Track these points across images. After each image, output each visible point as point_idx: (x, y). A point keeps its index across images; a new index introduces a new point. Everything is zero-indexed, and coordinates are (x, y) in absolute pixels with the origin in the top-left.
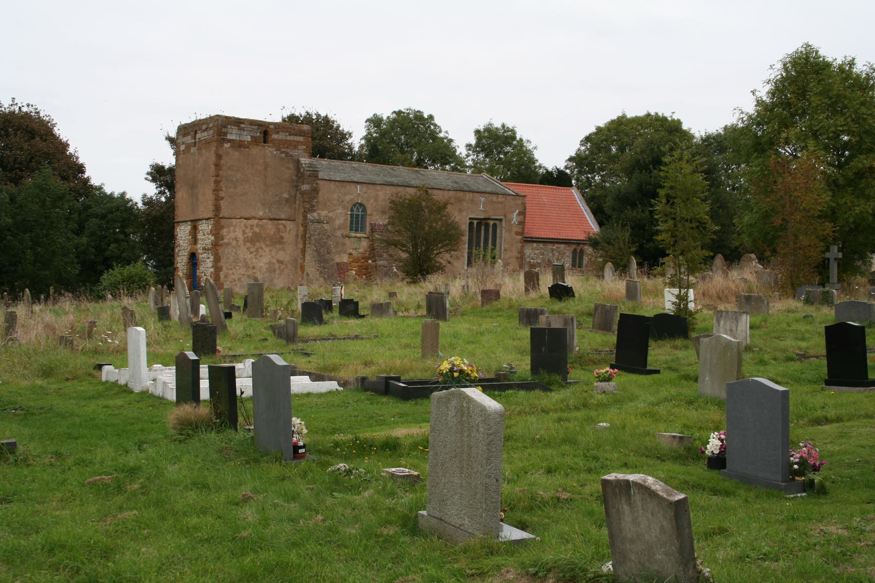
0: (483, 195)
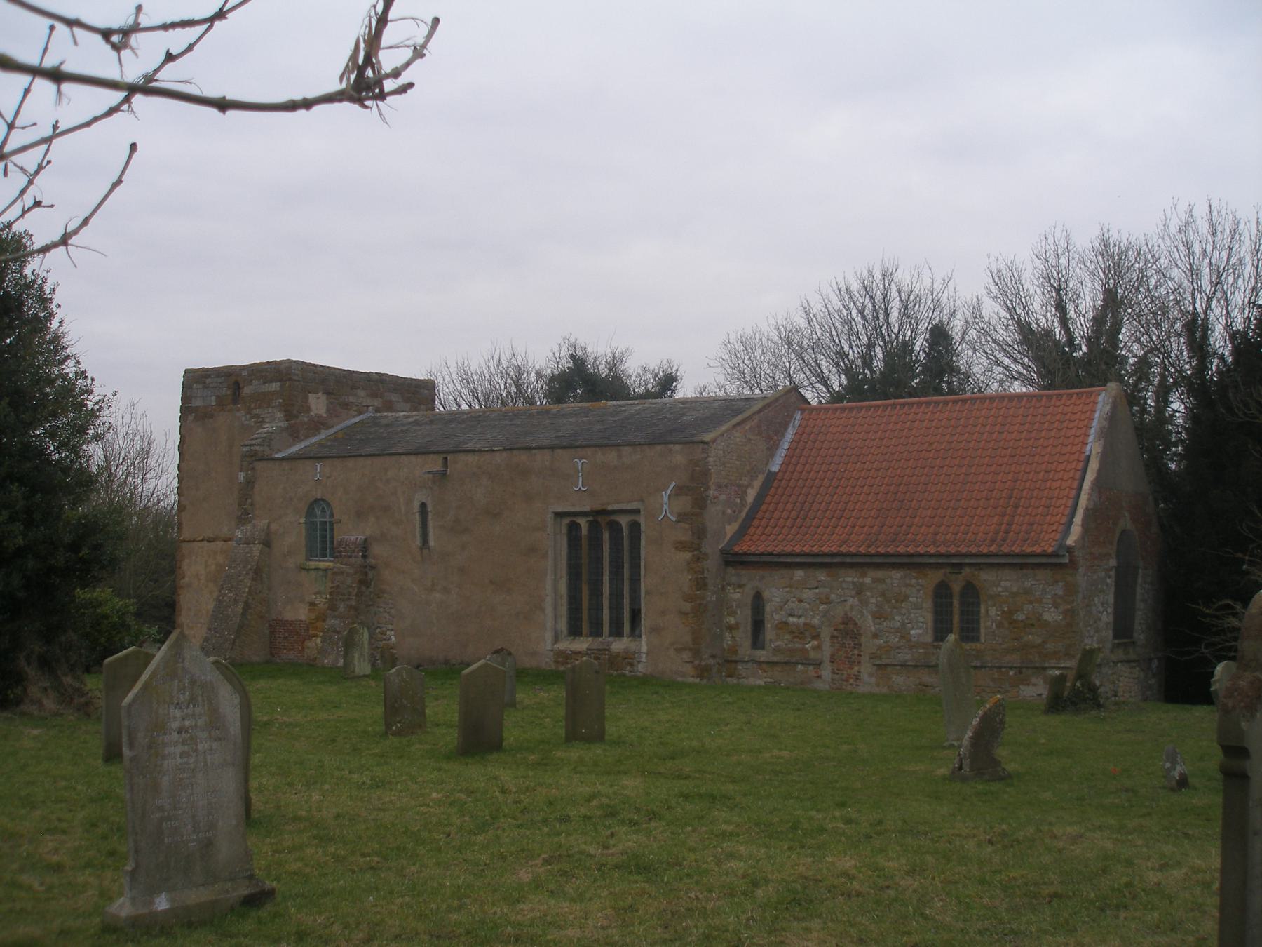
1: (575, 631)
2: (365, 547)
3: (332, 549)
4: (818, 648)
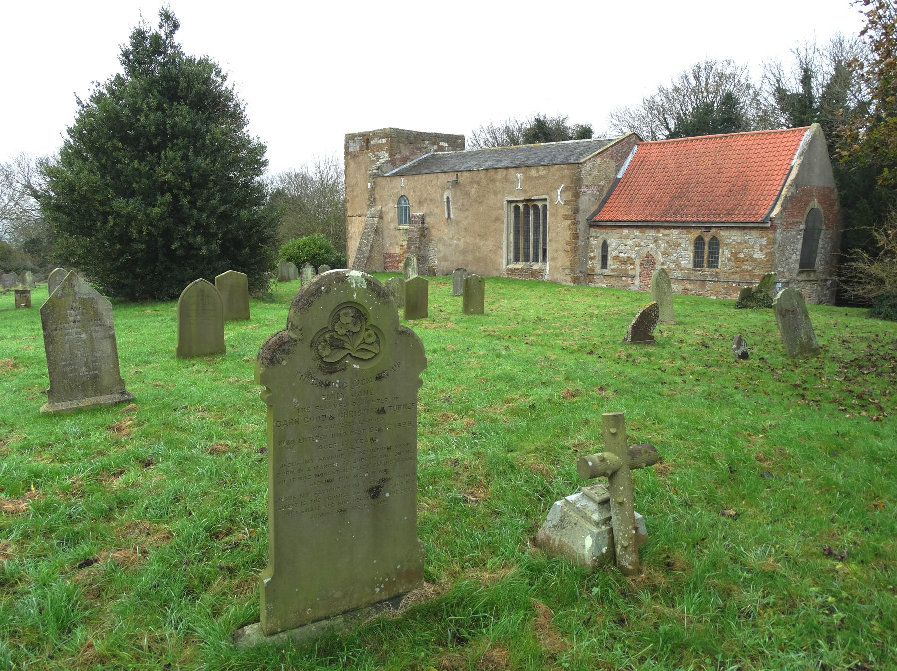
0: (520, 170)
1: (517, 259)
2: (423, 219)
3: (409, 219)
4: (633, 269)
